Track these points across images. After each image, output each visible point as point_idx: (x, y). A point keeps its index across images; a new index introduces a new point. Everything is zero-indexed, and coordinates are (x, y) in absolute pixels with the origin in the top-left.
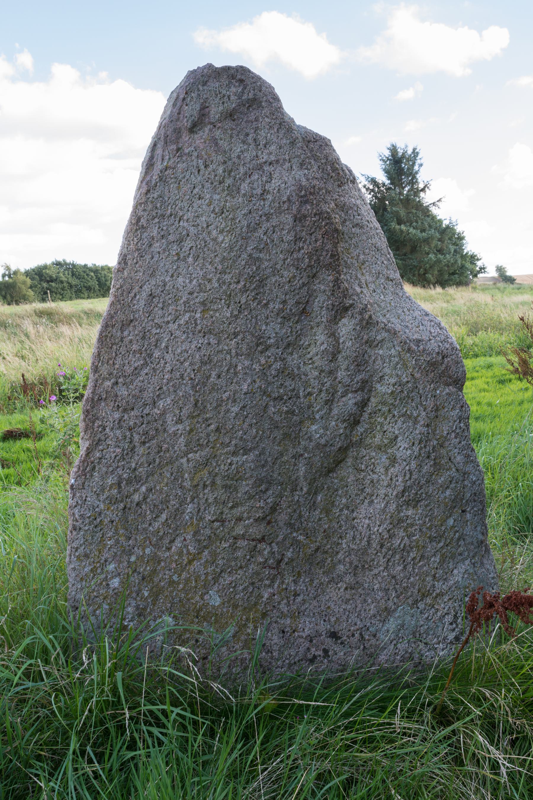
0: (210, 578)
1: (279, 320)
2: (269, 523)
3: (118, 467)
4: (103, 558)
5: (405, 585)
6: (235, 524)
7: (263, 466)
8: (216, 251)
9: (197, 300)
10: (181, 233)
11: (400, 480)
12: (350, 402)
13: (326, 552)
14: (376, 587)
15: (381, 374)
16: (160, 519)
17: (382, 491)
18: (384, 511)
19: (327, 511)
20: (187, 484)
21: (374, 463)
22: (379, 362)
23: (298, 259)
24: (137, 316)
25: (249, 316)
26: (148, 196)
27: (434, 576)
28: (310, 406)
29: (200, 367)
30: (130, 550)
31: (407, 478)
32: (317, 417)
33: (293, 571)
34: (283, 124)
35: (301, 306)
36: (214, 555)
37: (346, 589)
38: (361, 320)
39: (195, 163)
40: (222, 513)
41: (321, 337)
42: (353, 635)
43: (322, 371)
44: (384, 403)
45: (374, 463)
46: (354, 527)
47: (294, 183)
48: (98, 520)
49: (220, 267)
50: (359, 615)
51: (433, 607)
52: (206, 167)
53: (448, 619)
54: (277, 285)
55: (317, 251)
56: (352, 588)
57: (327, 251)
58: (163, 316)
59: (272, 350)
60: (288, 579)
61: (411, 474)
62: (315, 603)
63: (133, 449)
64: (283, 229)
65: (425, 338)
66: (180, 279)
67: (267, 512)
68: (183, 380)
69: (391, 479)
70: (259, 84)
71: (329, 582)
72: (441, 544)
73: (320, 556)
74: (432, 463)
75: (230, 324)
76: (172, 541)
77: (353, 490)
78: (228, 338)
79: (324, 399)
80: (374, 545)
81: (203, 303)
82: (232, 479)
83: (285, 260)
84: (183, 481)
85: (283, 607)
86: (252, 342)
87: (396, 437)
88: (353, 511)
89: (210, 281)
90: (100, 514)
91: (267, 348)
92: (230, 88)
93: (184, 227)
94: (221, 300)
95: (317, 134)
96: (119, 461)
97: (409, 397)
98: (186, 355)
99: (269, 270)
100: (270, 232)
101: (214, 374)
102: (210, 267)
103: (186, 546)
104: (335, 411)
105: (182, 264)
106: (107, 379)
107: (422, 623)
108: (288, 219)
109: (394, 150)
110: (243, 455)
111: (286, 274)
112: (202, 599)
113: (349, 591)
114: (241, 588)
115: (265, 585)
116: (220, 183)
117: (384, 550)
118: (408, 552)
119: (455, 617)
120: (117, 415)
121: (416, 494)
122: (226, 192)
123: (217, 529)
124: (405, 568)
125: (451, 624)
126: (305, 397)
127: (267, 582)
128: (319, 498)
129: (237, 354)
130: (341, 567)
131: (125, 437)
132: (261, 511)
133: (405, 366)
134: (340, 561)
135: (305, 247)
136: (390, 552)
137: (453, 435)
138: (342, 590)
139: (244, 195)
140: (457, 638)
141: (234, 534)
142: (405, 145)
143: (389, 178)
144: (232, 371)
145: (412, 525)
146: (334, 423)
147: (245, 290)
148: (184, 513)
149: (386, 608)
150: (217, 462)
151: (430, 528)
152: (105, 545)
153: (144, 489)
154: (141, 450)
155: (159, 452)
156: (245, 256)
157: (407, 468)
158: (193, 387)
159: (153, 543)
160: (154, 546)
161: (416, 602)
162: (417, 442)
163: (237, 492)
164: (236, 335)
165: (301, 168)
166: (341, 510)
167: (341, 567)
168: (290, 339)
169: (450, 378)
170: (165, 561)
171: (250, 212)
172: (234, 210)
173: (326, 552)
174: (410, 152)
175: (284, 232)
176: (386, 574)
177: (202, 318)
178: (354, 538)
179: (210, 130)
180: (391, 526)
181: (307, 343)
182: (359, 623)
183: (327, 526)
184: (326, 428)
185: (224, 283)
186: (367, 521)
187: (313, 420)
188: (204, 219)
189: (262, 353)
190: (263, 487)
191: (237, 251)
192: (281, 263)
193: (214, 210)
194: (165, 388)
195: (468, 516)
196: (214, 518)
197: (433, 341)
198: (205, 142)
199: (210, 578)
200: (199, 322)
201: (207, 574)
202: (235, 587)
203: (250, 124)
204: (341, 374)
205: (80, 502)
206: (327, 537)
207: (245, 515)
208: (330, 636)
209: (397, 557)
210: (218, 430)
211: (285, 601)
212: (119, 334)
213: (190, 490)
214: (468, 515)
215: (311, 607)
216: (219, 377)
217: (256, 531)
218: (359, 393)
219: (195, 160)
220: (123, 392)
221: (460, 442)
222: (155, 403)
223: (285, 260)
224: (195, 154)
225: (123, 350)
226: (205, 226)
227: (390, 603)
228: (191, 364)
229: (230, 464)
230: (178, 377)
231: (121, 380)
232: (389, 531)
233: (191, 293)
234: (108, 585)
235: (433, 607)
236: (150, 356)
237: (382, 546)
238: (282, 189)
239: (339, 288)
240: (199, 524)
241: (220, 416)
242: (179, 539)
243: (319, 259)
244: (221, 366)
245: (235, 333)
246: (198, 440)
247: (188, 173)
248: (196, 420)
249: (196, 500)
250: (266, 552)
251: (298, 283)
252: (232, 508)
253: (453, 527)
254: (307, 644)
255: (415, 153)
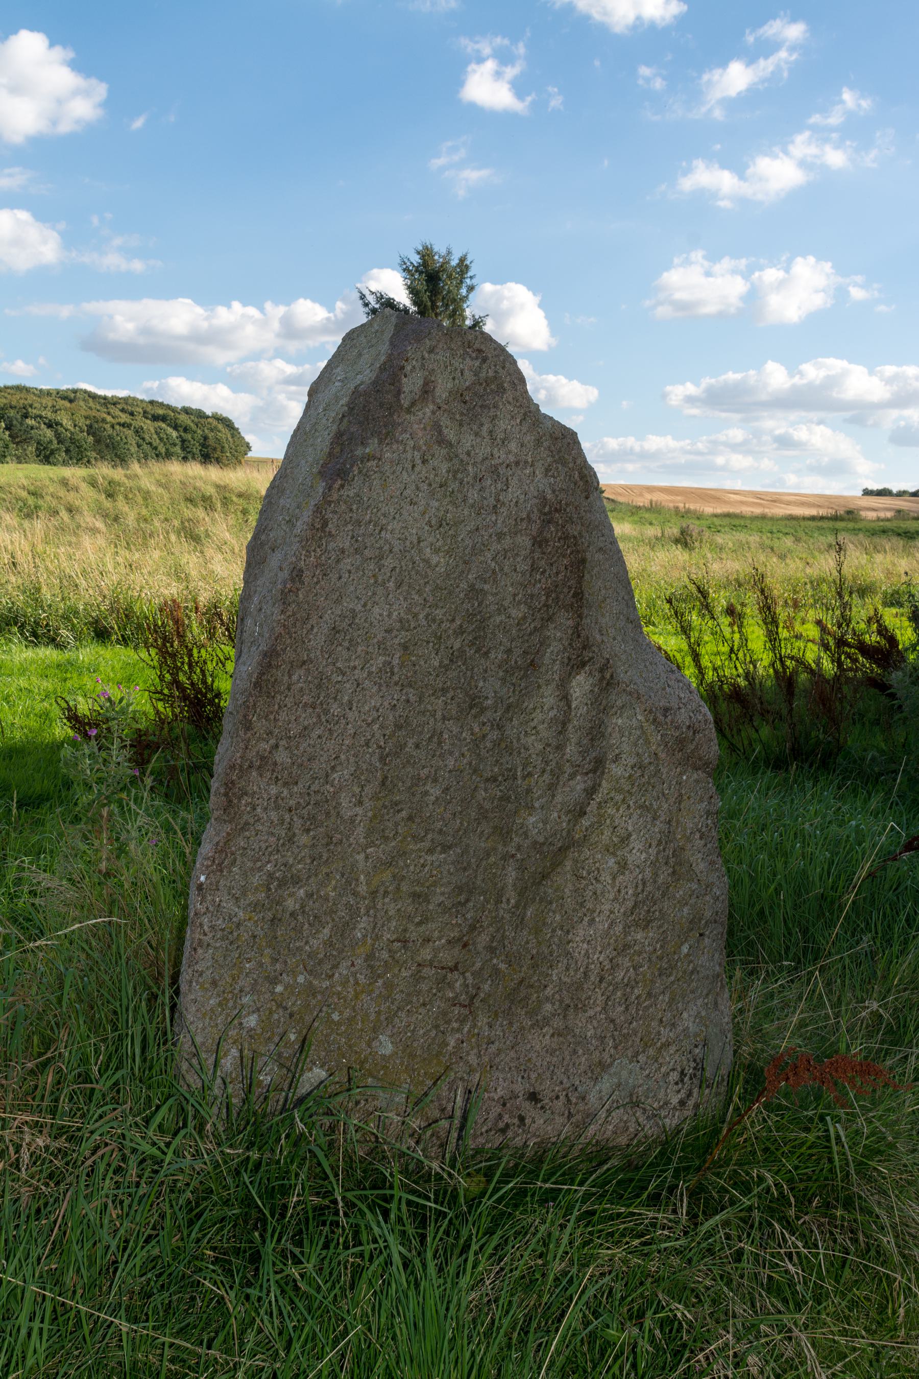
0: (383, 1017)
1: (501, 674)
2: (465, 945)
3: (269, 862)
4: (238, 987)
5: (625, 1031)
6: (422, 945)
7: (465, 869)
8: (427, 576)
9: (397, 641)
10: (381, 548)
11: (630, 892)
12: (578, 787)
13: (532, 986)
14: (589, 1034)
15: (617, 751)
16: (321, 936)
17: (606, 907)
18: (607, 934)
19: (537, 931)
20: (363, 889)
21: (598, 869)
22: (616, 735)
23: (532, 596)
24: (312, 656)
25: (463, 668)
26: (342, 492)
27: (661, 1021)
28: (529, 791)
29: (394, 732)
30: (276, 978)
31: (640, 889)
32: (537, 805)
33: (489, 1011)
34: (530, 413)
35: (529, 657)
36: (389, 986)
37: (553, 1035)
38: (603, 678)
39: (409, 456)
40: (405, 930)
41: (549, 697)
42: (557, 1097)
43: (548, 745)
44: (619, 790)
45: (598, 869)
46: (569, 953)
47: (536, 494)
48: (235, 934)
49: (431, 599)
50: (567, 1070)
51: (656, 1061)
52: (424, 462)
53: (674, 1076)
54: (502, 628)
55: (557, 586)
56: (560, 1035)
57: (570, 587)
58: (349, 660)
59: (489, 714)
60: (483, 1020)
61: (644, 884)
62: (512, 1054)
63: (291, 840)
64: (517, 554)
65: (674, 704)
66: (376, 610)
67: (465, 931)
68: (368, 747)
69: (619, 891)
70: (501, 358)
71: (532, 1026)
72: (672, 978)
73: (523, 993)
74: (671, 870)
75: (437, 676)
76: (335, 967)
77: (569, 903)
78: (433, 694)
79: (547, 781)
80: (592, 979)
81: (405, 647)
82: (422, 885)
83: (515, 595)
84: (357, 885)
85: (473, 1059)
86: (465, 702)
87: (630, 835)
88: (568, 932)
89: (415, 616)
90: (238, 925)
91: (483, 710)
92: (464, 359)
93: (386, 541)
94: (428, 642)
95: (564, 427)
96: (270, 854)
97: (649, 783)
98: (375, 714)
99: (493, 607)
100: (500, 558)
101: (411, 743)
102: (416, 597)
103: (354, 974)
104: (559, 798)
105: (380, 591)
106: (264, 739)
107: (641, 1082)
108: (524, 541)
109: (426, 254)
110: (441, 853)
111: (514, 612)
112: (369, 1046)
113: (555, 1039)
114: (421, 1032)
115: (453, 1029)
116: (441, 486)
117: (604, 985)
118: (632, 988)
119: (683, 1074)
120: (274, 790)
121: (649, 911)
122: (448, 499)
123: (396, 952)
124: (627, 1009)
125: (677, 1083)
126: (524, 778)
127: (455, 1025)
128: (529, 913)
129: (444, 718)
130: (548, 1007)
131: (282, 821)
132: (457, 929)
133: (647, 742)
134: (547, 999)
135: (543, 580)
136: (611, 988)
137: (697, 835)
138: (547, 1037)
139: (472, 506)
140: (682, 1103)
141: (419, 959)
142: (448, 245)
143: (415, 303)
144: (435, 740)
145: (640, 953)
146: (556, 814)
147: (461, 631)
148: (354, 928)
149: (600, 1062)
150: (405, 862)
151: (660, 958)
152: (241, 969)
153: (302, 892)
154: (304, 839)
155: (327, 845)
156: (464, 585)
157: (640, 877)
158: (382, 759)
159: (309, 968)
160: (310, 973)
161: (637, 1054)
162: (654, 844)
163: (429, 902)
164: (444, 691)
165: (546, 475)
166: (554, 931)
167: (548, 1007)
168: (511, 700)
169: (700, 759)
170: (323, 993)
171: (477, 529)
172: (457, 523)
173: (532, 986)
174: (454, 262)
175: (519, 559)
176: (603, 1016)
177: (402, 665)
178: (567, 969)
179: (433, 413)
180: (615, 953)
181: (531, 706)
182: (565, 1080)
183: (534, 952)
184: (545, 822)
185: (434, 620)
186: (585, 946)
187: (531, 808)
188: (414, 531)
189: (475, 717)
190: (462, 898)
191: (455, 579)
192: (510, 598)
193: (429, 521)
194: (343, 757)
195: (707, 941)
196: (394, 937)
197: (683, 710)
198: (425, 429)
199: (383, 1017)
200: (396, 670)
201: (378, 1013)
202: (414, 1031)
203: (486, 411)
204: (571, 750)
205: (211, 909)
206: (535, 966)
207: (436, 934)
208: (528, 1099)
209: (619, 994)
210: (410, 818)
211: (475, 1051)
212: (286, 678)
213: (365, 898)
214: (706, 940)
215: (507, 1059)
216: (417, 746)
217: (447, 957)
218: (590, 775)
219: (410, 451)
220: (282, 757)
221: (706, 845)
222: (327, 776)
223: (515, 595)
224: (411, 443)
225: (289, 701)
226: (415, 541)
227: (606, 1056)
228: (382, 727)
229: (423, 866)
230: (362, 743)
231: (283, 743)
232: (611, 961)
233: (388, 631)
234: (241, 1024)
235: (656, 1061)
236: (326, 711)
237: (601, 981)
238: (521, 501)
239: (579, 636)
240: (373, 945)
241: (415, 800)
242: (345, 964)
243: (557, 598)
244: (421, 733)
245: (443, 689)
246: (383, 831)
247: (399, 468)
248: (381, 803)
249: (372, 912)
250: (458, 984)
251: (528, 626)
252: (419, 924)
253: (688, 955)
254: (499, 1109)
255: (463, 267)
